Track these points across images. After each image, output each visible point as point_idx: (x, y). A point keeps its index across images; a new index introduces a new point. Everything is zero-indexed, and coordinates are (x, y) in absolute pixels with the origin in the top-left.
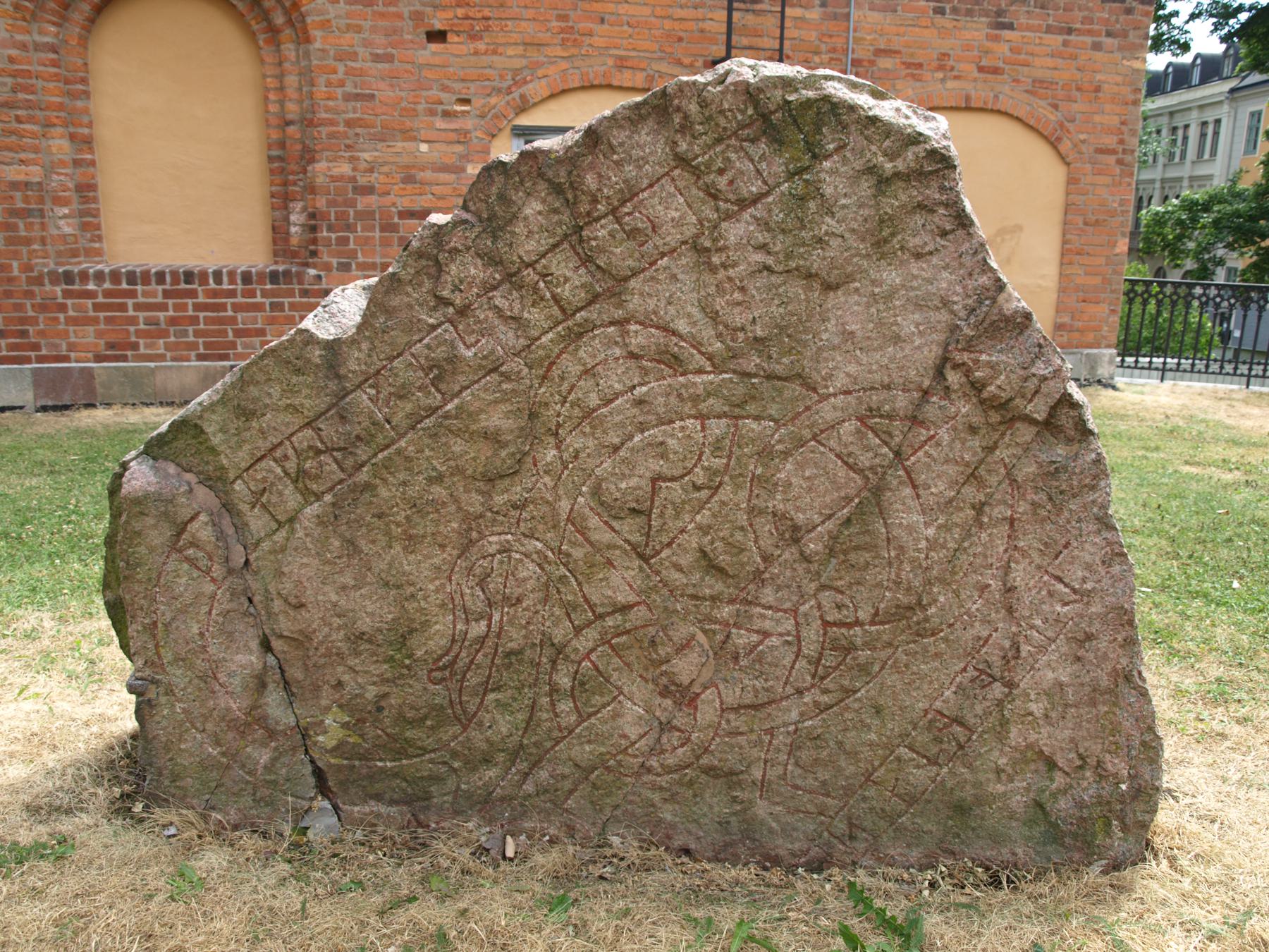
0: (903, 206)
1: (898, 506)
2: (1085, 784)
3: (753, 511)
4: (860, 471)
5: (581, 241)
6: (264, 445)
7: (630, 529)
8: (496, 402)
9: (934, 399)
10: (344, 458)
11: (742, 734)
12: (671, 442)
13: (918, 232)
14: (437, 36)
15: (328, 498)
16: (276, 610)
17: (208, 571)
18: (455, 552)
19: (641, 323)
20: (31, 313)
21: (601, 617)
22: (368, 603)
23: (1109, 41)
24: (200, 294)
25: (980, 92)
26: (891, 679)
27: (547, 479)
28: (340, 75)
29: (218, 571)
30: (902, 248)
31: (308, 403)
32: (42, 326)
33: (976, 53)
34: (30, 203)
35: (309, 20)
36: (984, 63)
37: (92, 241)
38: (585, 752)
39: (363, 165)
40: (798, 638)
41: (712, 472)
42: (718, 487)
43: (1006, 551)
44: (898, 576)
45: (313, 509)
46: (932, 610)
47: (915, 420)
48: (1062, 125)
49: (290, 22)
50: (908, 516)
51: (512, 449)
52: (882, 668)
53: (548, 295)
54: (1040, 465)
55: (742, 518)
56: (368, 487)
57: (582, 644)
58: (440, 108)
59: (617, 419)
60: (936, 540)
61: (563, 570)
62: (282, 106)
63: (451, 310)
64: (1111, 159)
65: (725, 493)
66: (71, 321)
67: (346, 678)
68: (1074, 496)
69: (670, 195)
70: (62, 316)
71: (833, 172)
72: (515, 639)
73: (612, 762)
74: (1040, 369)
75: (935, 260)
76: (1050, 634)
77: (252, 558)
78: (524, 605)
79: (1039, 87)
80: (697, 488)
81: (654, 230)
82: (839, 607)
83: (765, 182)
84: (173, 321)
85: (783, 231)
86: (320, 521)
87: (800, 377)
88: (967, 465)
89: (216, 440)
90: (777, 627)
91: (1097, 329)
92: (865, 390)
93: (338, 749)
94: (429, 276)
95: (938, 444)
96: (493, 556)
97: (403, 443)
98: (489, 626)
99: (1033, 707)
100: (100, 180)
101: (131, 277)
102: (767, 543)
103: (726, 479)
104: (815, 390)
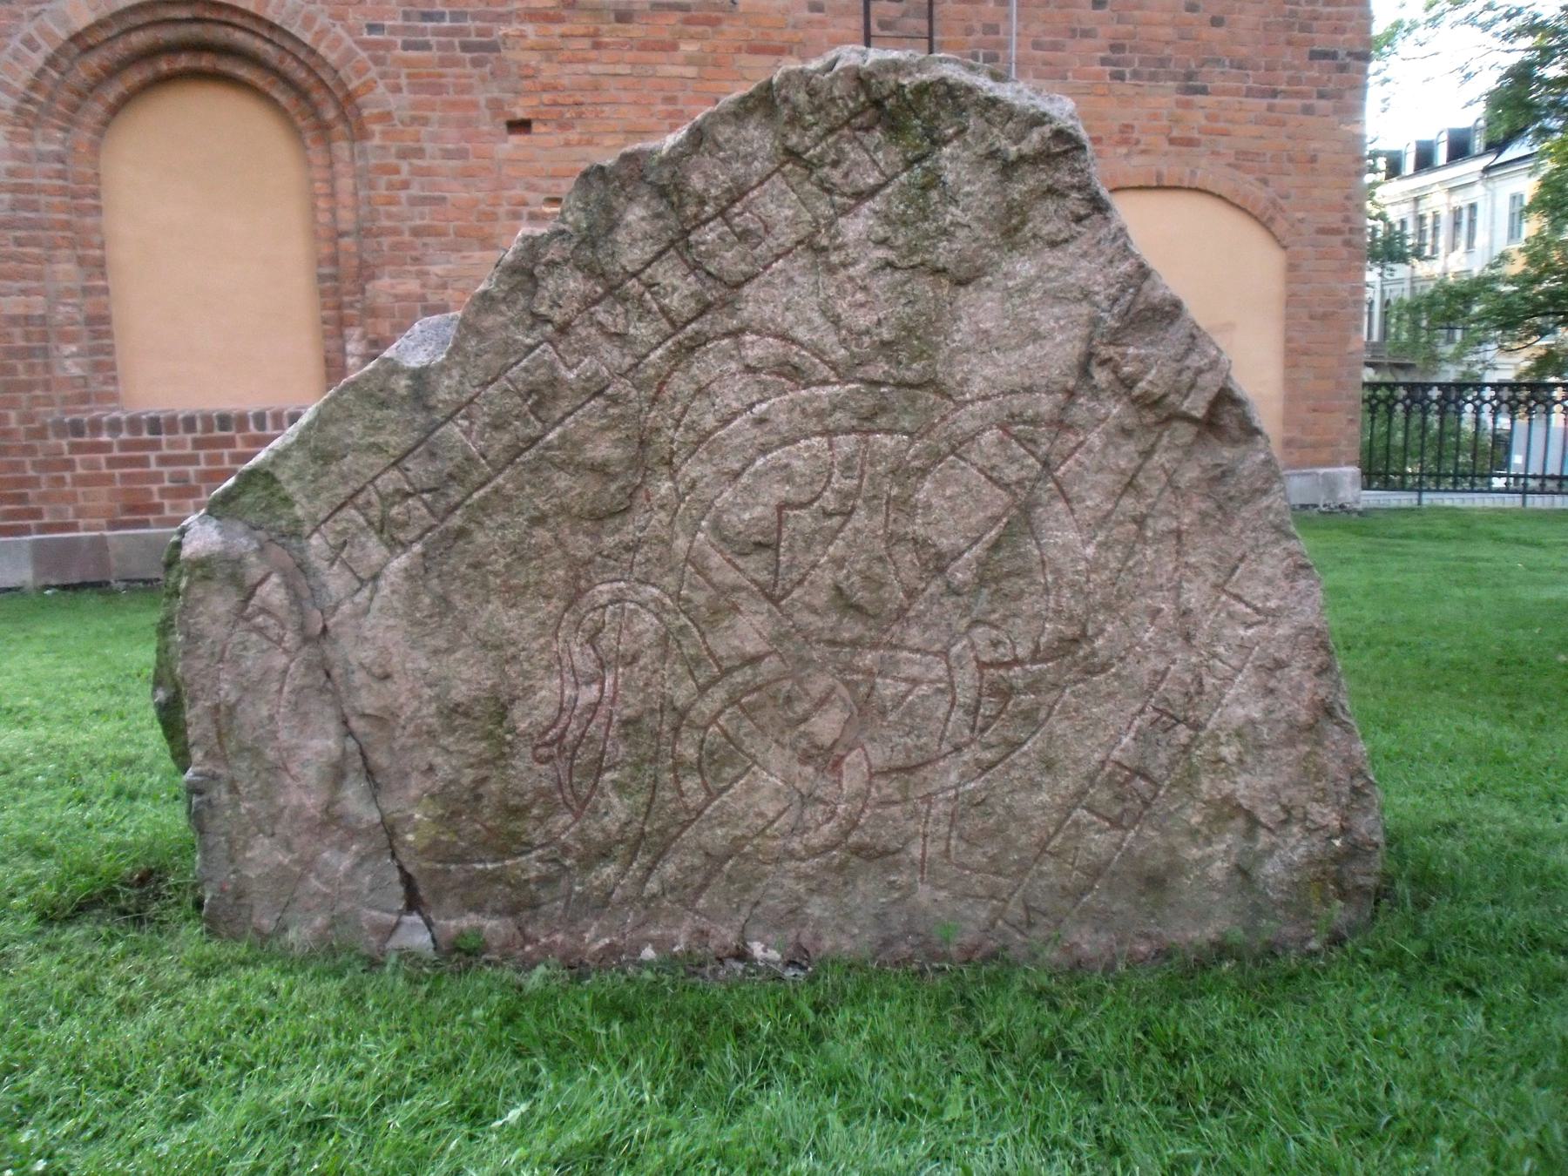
0: (1032, 191)
1: (1051, 524)
2: (1292, 841)
3: (893, 539)
4: (1006, 486)
5: (688, 246)
6: (344, 491)
7: (756, 566)
8: (603, 429)
10: (435, 500)
11: (895, 803)
12: (797, 464)
13: (1047, 220)
14: (520, 126)
18: (562, 604)
19: (758, 333)
20: (31, 473)
21: (728, 672)
22: (463, 668)
23: (1323, 103)
25: (1172, 169)
26: (1061, 727)
27: (662, 515)
29: (290, 639)
30: (1035, 236)
31: (393, 440)
32: (44, 488)
33: (1165, 122)
35: (366, 113)
36: (1175, 133)
37: (105, 383)
38: (718, 837)
39: (433, 280)
40: (952, 684)
41: (844, 496)
42: (851, 512)
43: (1176, 569)
44: (1058, 603)
45: (401, 561)
46: (1099, 642)
47: (1061, 425)
48: (1274, 203)
49: (342, 116)
50: (1063, 537)
53: (655, 307)
54: (1204, 470)
56: (462, 533)
57: (707, 706)
58: (525, 210)
59: (737, 441)
60: (1096, 560)
61: (683, 620)
62: (334, 215)
63: (549, 328)
64: (1337, 240)
65: (860, 519)
67: (439, 760)
68: (1246, 502)
69: (784, 192)
70: (68, 475)
71: (953, 158)
73: (748, 848)
74: (1195, 360)
75: (1071, 248)
76: (1234, 662)
77: (330, 623)
78: (641, 663)
80: (828, 515)
81: (767, 231)
82: (995, 644)
83: (882, 173)
85: (905, 223)
86: (409, 575)
87: (929, 383)
88: (1123, 472)
89: (291, 488)
90: (927, 671)
92: (1004, 393)
93: (433, 849)
94: (526, 292)
96: (604, 607)
97: (500, 480)
98: (602, 691)
99: (1225, 751)
100: (115, 312)
101: (155, 425)
102: (910, 575)
103: (859, 502)
104: (950, 397)
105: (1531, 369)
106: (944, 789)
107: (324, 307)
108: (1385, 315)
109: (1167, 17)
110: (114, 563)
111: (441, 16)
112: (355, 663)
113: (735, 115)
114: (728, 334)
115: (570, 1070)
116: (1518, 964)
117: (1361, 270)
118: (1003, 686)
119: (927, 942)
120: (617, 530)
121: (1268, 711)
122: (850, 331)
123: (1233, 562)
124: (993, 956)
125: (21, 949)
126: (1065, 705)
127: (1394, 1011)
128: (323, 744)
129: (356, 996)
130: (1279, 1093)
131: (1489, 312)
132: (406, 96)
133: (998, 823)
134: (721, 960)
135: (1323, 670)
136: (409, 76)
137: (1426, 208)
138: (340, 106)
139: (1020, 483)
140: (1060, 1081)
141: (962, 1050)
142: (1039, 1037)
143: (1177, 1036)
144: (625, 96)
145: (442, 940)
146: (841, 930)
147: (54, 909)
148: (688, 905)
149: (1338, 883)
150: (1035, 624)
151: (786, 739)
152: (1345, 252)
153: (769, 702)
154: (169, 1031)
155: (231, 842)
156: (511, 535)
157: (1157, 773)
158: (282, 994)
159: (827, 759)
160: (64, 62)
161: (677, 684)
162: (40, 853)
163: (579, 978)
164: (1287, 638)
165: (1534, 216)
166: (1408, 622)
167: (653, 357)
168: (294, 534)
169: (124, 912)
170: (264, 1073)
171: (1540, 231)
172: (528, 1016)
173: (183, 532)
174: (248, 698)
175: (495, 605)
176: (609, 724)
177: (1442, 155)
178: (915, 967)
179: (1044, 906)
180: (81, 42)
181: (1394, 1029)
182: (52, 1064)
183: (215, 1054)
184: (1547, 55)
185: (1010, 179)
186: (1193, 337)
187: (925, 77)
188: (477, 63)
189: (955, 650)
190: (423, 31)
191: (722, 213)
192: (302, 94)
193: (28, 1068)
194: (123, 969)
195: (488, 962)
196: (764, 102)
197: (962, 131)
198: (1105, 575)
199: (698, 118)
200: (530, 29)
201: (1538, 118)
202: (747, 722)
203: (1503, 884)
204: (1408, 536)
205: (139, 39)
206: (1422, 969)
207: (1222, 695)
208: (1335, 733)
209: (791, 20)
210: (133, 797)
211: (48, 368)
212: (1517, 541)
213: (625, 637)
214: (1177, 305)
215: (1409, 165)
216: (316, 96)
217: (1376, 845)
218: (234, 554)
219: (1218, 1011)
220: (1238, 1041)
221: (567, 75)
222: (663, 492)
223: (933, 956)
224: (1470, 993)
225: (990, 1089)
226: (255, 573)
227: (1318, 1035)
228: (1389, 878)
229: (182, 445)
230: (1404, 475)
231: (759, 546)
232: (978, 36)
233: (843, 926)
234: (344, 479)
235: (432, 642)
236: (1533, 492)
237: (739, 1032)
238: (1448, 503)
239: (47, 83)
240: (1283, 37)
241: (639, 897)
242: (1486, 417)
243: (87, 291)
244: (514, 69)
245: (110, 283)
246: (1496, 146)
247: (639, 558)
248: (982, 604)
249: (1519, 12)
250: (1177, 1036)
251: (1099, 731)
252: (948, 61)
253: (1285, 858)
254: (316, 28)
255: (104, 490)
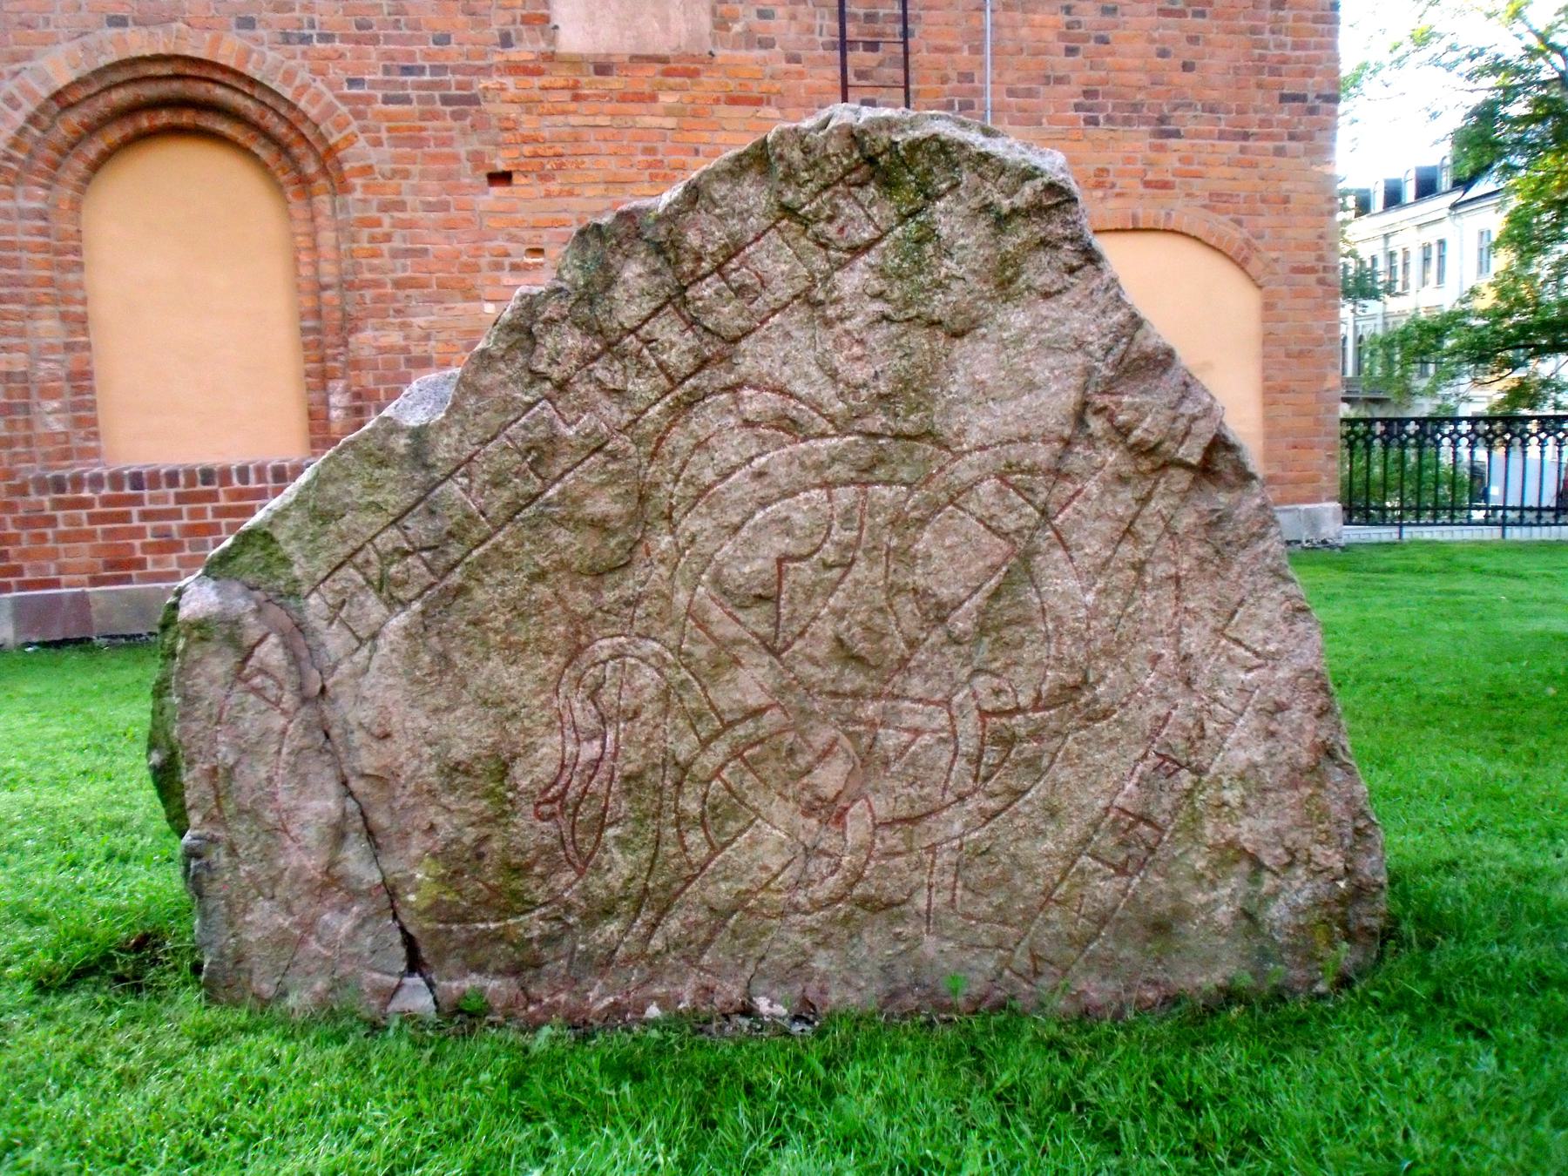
2: (1297, 884)
3: (893, 590)
5: (686, 303)
6: (342, 550)
7: (756, 619)
8: (602, 485)
9: (1078, 449)
10: (435, 558)
11: (899, 854)
12: (797, 517)
13: (1040, 271)
14: (501, 178)
15: (417, 606)
16: (356, 744)
17: (277, 703)
18: (562, 660)
19: (755, 387)
21: (730, 725)
23: (1293, 144)
24: (222, 496)
25: (1148, 211)
26: (1064, 774)
27: (663, 570)
28: (386, 228)
29: (289, 700)
30: (1029, 288)
31: (392, 499)
32: (25, 546)
33: (1139, 166)
34: (20, 393)
35: (346, 167)
36: (1150, 176)
37: (87, 439)
38: (722, 892)
39: (417, 332)
40: (954, 734)
41: (846, 547)
45: (400, 620)
46: (1101, 689)
47: (1058, 473)
49: (324, 171)
50: (1062, 585)
51: (620, 538)
52: (1052, 762)
53: (653, 364)
54: (1201, 516)
55: (880, 598)
56: (462, 590)
57: (710, 760)
58: (507, 261)
59: (737, 495)
61: (684, 674)
62: (316, 269)
63: (548, 385)
65: (860, 570)
66: (64, 537)
67: (440, 820)
68: (1244, 547)
69: (779, 248)
70: (49, 532)
71: (947, 212)
72: (634, 760)
73: (752, 903)
74: (1189, 408)
75: (1065, 299)
77: (329, 683)
79: (1217, 201)
80: (828, 567)
82: (997, 693)
84: (190, 531)
85: (900, 277)
86: (408, 634)
87: (928, 435)
88: (1121, 519)
89: (290, 549)
90: (929, 721)
91: (1314, 480)
92: (1001, 443)
93: (436, 909)
95: (1087, 499)
96: (605, 662)
97: (500, 537)
98: (603, 747)
99: (1228, 795)
100: (96, 366)
101: (137, 480)
102: (910, 624)
103: (859, 553)
104: (947, 448)
105: (1503, 402)
106: (948, 839)
107: (307, 360)
108: (1359, 351)
109: (1138, 63)
110: (96, 620)
111: (422, 70)
112: (354, 725)
113: (730, 172)
114: (726, 389)
115: (583, 1133)
116: (1527, 1004)
117: (1336, 307)
118: (1007, 734)
119: (934, 993)
120: (617, 586)
121: (1270, 754)
122: (847, 384)
123: (1232, 607)
124: (1001, 1006)
125: (17, 1020)
126: (1067, 752)
127: (1406, 1054)
128: (323, 805)
129: (359, 1062)
130: (1297, 1141)
131: (1462, 346)
132: (387, 150)
133: (1003, 873)
134: (727, 1017)
135: (1323, 712)
136: (389, 130)
137: (1395, 244)
138: (321, 160)
139: (1018, 531)
140: (1077, 1134)
141: (976, 1103)
142: (1053, 1089)
143: (1191, 1084)
144: (604, 147)
145: (444, 1002)
146: (848, 983)
147: (50, 977)
148: (692, 961)
149: (1344, 925)
150: (1036, 672)
151: (790, 792)
152: (1319, 290)
153: (770, 753)
154: (171, 1104)
155: (230, 905)
156: (511, 592)
157: (1161, 818)
158: (284, 1060)
159: (831, 811)
160: (45, 120)
161: (679, 738)
162: (34, 920)
163: (585, 1037)
164: (1288, 681)
165: (1501, 251)
166: (1398, 657)
167: (652, 412)
168: (292, 594)
169: (119, 979)
170: (270, 1145)
171: (1510, 265)
172: (537, 1079)
173: (180, 593)
174: (246, 760)
175: (495, 662)
176: (611, 780)
177: (1409, 193)
178: (922, 1019)
179: (1051, 954)
180: (60, 98)
181: (1407, 1072)
182: (53, 1138)
183: (218, 1126)
184: (1510, 93)
185: (1003, 232)
186: (1186, 384)
187: (918, 134)
188: (457, 116)
189: (957, 699)
190: (403, 85)
191: (719, 268)
192: (282, 148)
193: (28, 1144)
194: (121, 1038)
195: (492, 1024)
196: (759, 159)
197: (955, 186)
198: (1106, 621)
199: (694, 175)
200: (509, 81)
201: (1502, 155)
202: (750, 776)
203: (1508, 922)
204: (1390, 570)
205: (121, 96)
206: (1431, 1011)
207: (1224, 739)
208: (1337, 775)
209: (768, 71)
210: (125, 860)
211: (29, 424)
212: (1499, 573)
213: (626, 693)
214: (1170, 353)
215: (1378, 202)
216: (297, 151)
217: (1381, 886)
218: (232, 615)
219: (1232, 1057)
220: (1253, 1088)
221: (546, 127)
222: (663, 546)
223: (941, 1007)
224: (1481, 1035)
225: (1008, 1144)
226: (253, 634)
227: (1332, 1080)
228: (1394, 920)
229: (165, 499)
230: (1384, 510)
231: (760, 598)
232: (954, 84)
233: (850, 978)
234: (343, 538)
235: (432, 701)
236: (1513, 524)
237: (749, 1089)
238: (1427, 536)
239: (27, 141)
240: (1253, 81)
241: (643, 955)
242: (1464, 452)
243: (69, 347)
244: (494, 122)
245: (92, 339)
246: (1463, 183)
247: (639, 612)
248: (983, 653)
249: (1481, 52)
250: (1191, 1084)
251: (1101, 776)
252: (939, 117)
253: (1291, 900)
254: (297, 82)
255: (84, 546)
